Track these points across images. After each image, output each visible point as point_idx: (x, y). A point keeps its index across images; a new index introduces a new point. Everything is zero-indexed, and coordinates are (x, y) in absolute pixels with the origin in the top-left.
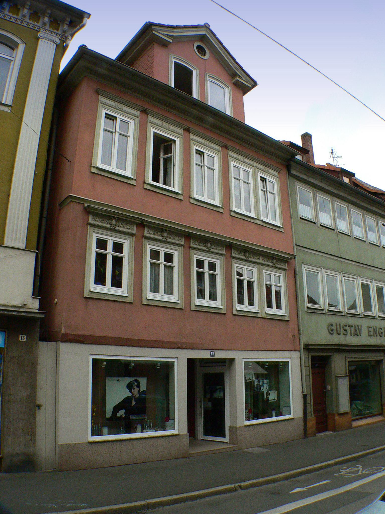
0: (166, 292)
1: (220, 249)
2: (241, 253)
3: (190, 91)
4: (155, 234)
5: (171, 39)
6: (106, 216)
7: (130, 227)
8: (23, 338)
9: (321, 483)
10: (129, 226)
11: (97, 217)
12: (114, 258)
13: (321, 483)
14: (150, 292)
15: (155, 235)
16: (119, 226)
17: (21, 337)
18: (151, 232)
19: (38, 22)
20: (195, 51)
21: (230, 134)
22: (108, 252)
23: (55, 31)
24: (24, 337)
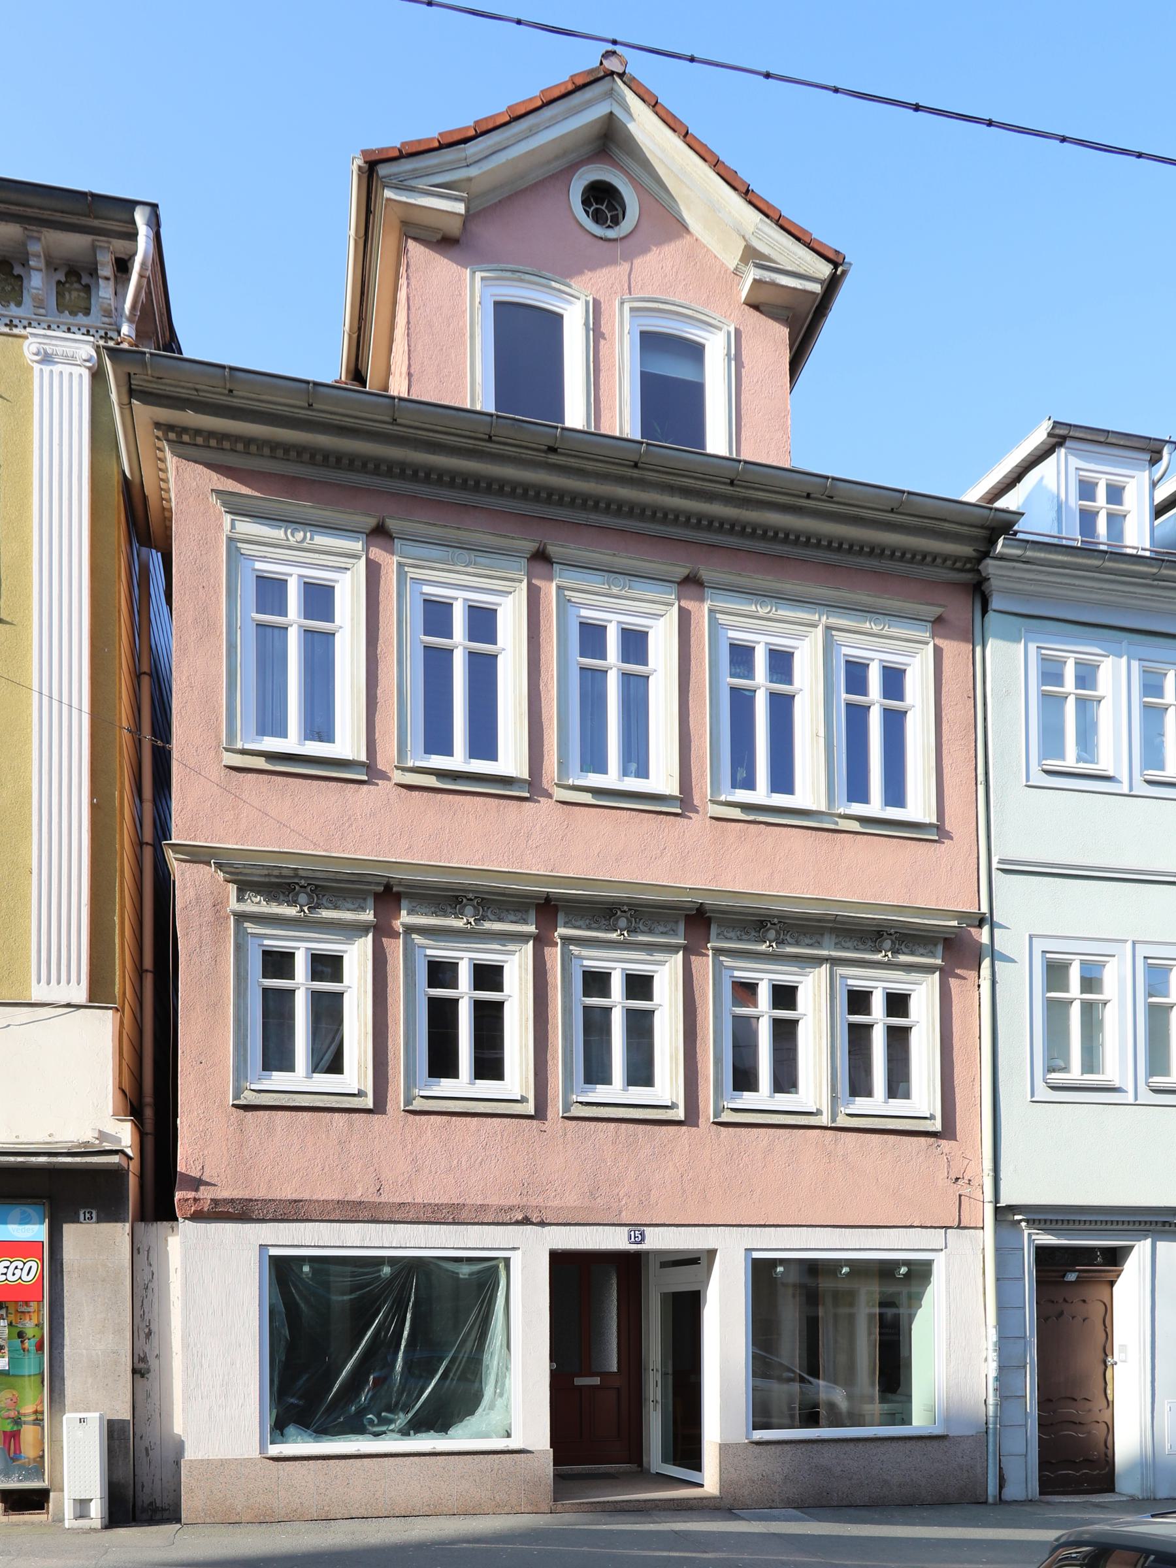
0: (317, 1066)
1: (665, 930)
2: (864, 943)
3: (696, 431)
4: (593, 926)
5: (456, 199)
6: (279, 885)
7: (356, 906)
8: (88, 1215)
9: (682, 1554)
10: (666, 927)
11: (848, 939)
12: (631, 1014)
13: (682, 1554)
14: (263, 1070)
15: (740, 940)
16: (638, 930)
17: (84, 1213)
18: (729, 935)
19: (19, 304)
20: (578, 222)
21: (313, 456)
22: (655, 1005)
23: (81, 319)
24: (92, 1213)
